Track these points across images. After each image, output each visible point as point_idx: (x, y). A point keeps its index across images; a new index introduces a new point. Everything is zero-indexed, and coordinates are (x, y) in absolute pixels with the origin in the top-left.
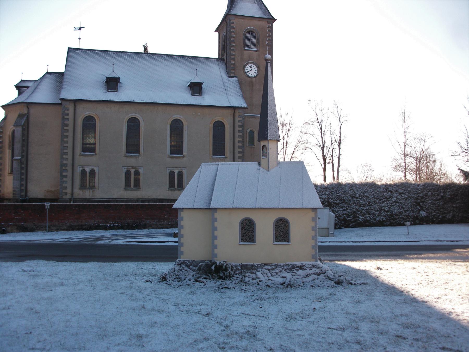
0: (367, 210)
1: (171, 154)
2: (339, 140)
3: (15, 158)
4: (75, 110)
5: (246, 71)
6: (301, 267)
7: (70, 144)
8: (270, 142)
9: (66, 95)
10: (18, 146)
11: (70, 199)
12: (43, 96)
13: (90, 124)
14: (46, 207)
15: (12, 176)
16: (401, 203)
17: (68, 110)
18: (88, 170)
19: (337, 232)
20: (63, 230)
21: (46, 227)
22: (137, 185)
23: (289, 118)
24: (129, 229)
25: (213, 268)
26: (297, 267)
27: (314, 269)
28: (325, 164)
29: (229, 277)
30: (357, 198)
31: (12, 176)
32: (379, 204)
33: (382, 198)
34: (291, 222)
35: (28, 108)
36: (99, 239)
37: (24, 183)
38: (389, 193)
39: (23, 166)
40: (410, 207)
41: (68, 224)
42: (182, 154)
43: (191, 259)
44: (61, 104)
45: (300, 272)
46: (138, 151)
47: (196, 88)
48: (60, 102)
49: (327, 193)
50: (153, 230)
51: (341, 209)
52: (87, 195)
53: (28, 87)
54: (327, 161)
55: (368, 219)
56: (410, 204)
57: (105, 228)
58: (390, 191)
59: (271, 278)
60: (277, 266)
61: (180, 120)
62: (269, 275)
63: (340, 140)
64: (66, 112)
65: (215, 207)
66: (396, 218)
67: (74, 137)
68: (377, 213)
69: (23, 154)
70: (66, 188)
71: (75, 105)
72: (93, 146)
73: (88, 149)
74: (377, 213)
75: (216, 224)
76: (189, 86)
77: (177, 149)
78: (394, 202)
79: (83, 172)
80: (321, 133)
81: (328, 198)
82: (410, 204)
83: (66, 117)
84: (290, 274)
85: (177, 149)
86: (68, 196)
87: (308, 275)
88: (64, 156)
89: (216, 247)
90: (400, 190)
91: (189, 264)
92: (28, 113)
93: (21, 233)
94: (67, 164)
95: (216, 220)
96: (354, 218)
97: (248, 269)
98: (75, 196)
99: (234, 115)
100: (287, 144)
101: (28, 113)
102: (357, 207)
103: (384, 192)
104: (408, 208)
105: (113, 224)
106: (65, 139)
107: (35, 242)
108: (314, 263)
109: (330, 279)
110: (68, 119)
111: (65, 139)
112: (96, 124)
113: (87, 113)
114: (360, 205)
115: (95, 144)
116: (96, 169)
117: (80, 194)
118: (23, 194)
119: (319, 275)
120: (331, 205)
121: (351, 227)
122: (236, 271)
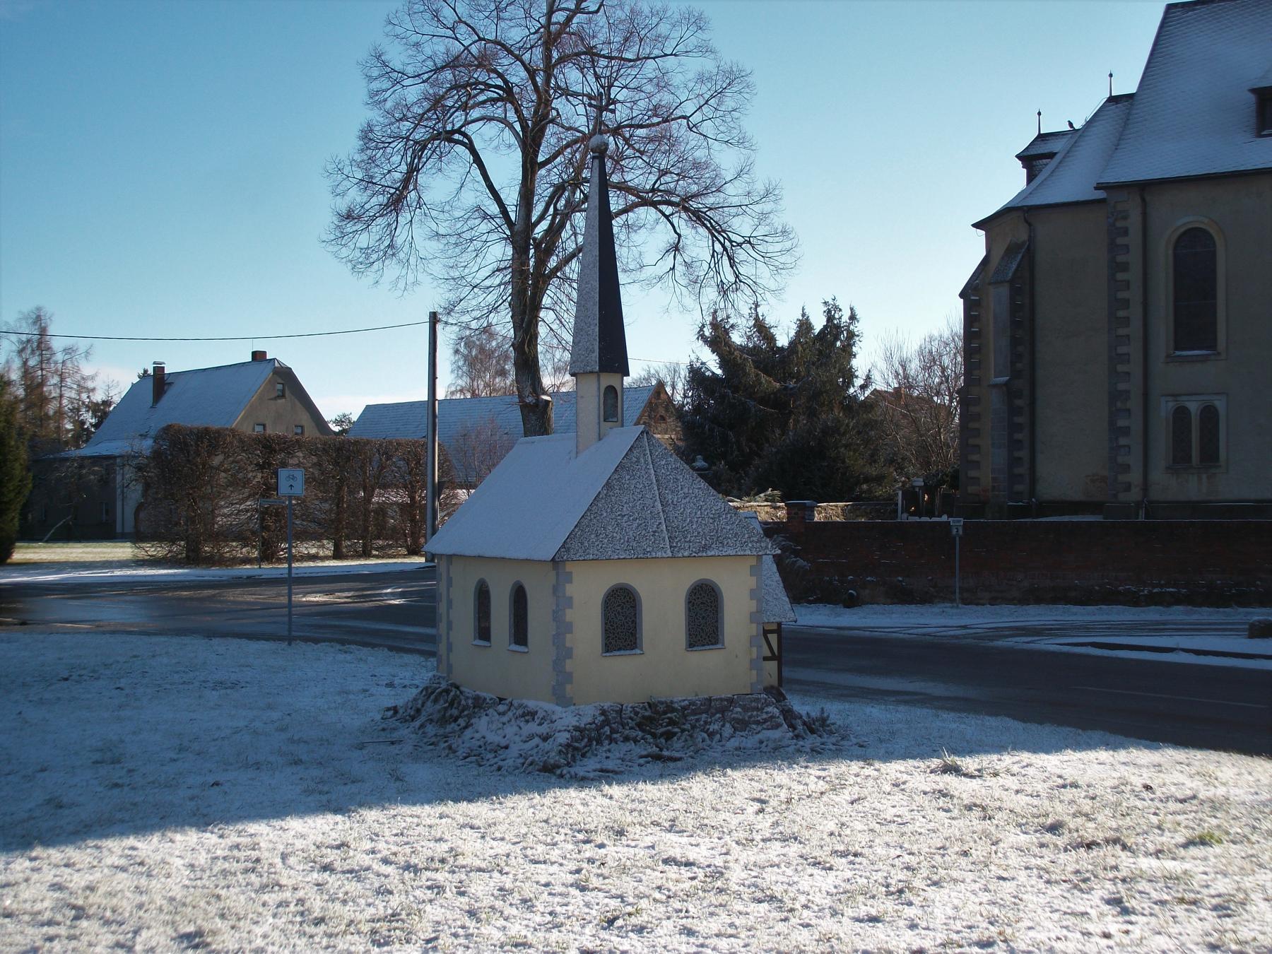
1: (1176, 349)
4: (1145, 215)
7: (1135, 329)
14: (954, 531)
17: (1125, 218)
18: (1194, 407)
22: (1210, 456)
24: (1210, 605)
35: (1030, 224)
36: (999, 633)
37: (1024, 454)
46: (1209, 341)
48: (1100, 194)
52: (1193, 488)
53: (1051, 155)
64: (1119, 224)
69: (1019, 365)
70: (1126, 468)
71: (1143, 200)
79: (1181, 414)
83: (1120, 241)
86: (1135, 495)
92: (1031, 239)
94: (1128, 392)
101: (1031, 239)
105: (1162, 586)
106: (1121, 314)
107: (842, 632)
110: (1127, 246)
111: (1121, 314)
113: (1185, 221)
116: (1220, 404)
117: (1172, 486)
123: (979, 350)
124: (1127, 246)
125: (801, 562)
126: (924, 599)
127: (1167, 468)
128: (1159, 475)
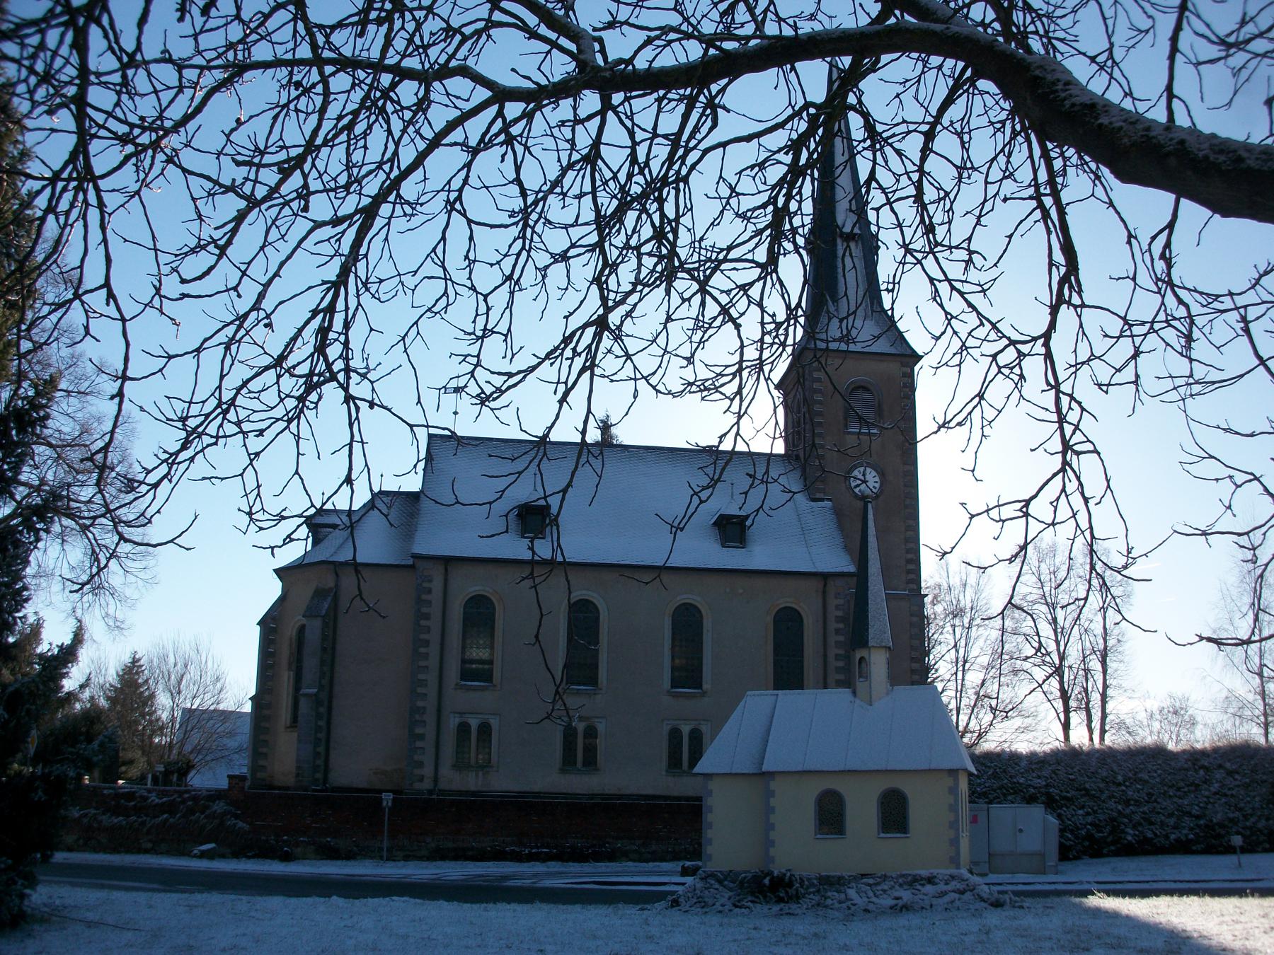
0: (1144, 813)
2: (1101, 646)
3: (304, 691)
5: (853, 484)
6: (931, 880)
7: (433, 662)
8: (873, 651)
9: (423, 546)
10: (311, 664)
11: (430, 792)
12: (374, 546)
13: (480, 614)
14: (385, 803)
15: (295, 735)
16: (1232, 795)
18: (474, 723)
19: (1067, 865)
20: (421, 858)
21: (381, 849)
22: (591, 761)
24: (574, 861)
25: (767, 881)
26: (922, 879)
27: (954, 883)
28: (1067, 711)
29: (797, 898)
30: (1119, 784)
31: (295, 735)
32: (1175, 800)
33: (1182, 784)
34: (909, 796)
35: (337, 575)
36: (506, 878)
37: (321, 749)
38: (1202, 772)
39: (322, 710)
40: (1257, 805)
41: (433, 845)
42: (699, 686)
43: (726, 869)
44: (412, 567)
45: (929, 888)
47: (732, 529)
48: (410, 562)
49: (1045, 773)
50: (630, 864)
51: (1081, 812)
52: (471, 782)
54: (1073, 704)
55: (1150, 835)
56: (1257, 799)
57: (517, 858)
58: (1203, 767)
59: (874, 899)
60: (885, 877)
61: (696, 607)
62: (870, 894)
63: (1106, 647)
64: (425, 585)
65: (771, 769)
66: (1223, 832)
67: (442, 644)
68: (1172, 821)
69: (323, 682)
71: (446, 570)
72: (486, 667)
73: (478, 674)
74: (1172, 821)
75: (773, 802)
76: (715, 524)
77: (688, 675)
78: (1216, 793)
79: (464, 729)
80: (1055, 631)
81: (1047, 786)
82: (1257, 799)
84: (909, 892)
85: (688, 675)
86: (427, 785)
87: (943, 894)
88: (419, 690)
89: (772, 843)
90: (1228, 765)
91: (722, 878)
92: (337, 586)
93: (325, 862)
94: (424, 708)
95: (772, 794)
96: (1111, 833)
97: (831, 884)
98: (443, 785)
99: (824, 592)
100: (965, 662)
102: (1120, 807)
103: (1187, 770)
104: (1253, 809)
108: (954, 871)
109: (983, 900)
111: (422, 650)
112: (494, 615)
114: (1127, 803)
115: (491, 662)
116: (494, 722)
117: (456, 781)
118: (319, 776)
119: (962, 892)
120: (1055, 801)
121: (1108, 855)
122: (808, 888)
123: (272, 666)
124: (430, 602)
125: (240, 824)
126: (350, 856)
127: (454, 766)
128: (446, 771)
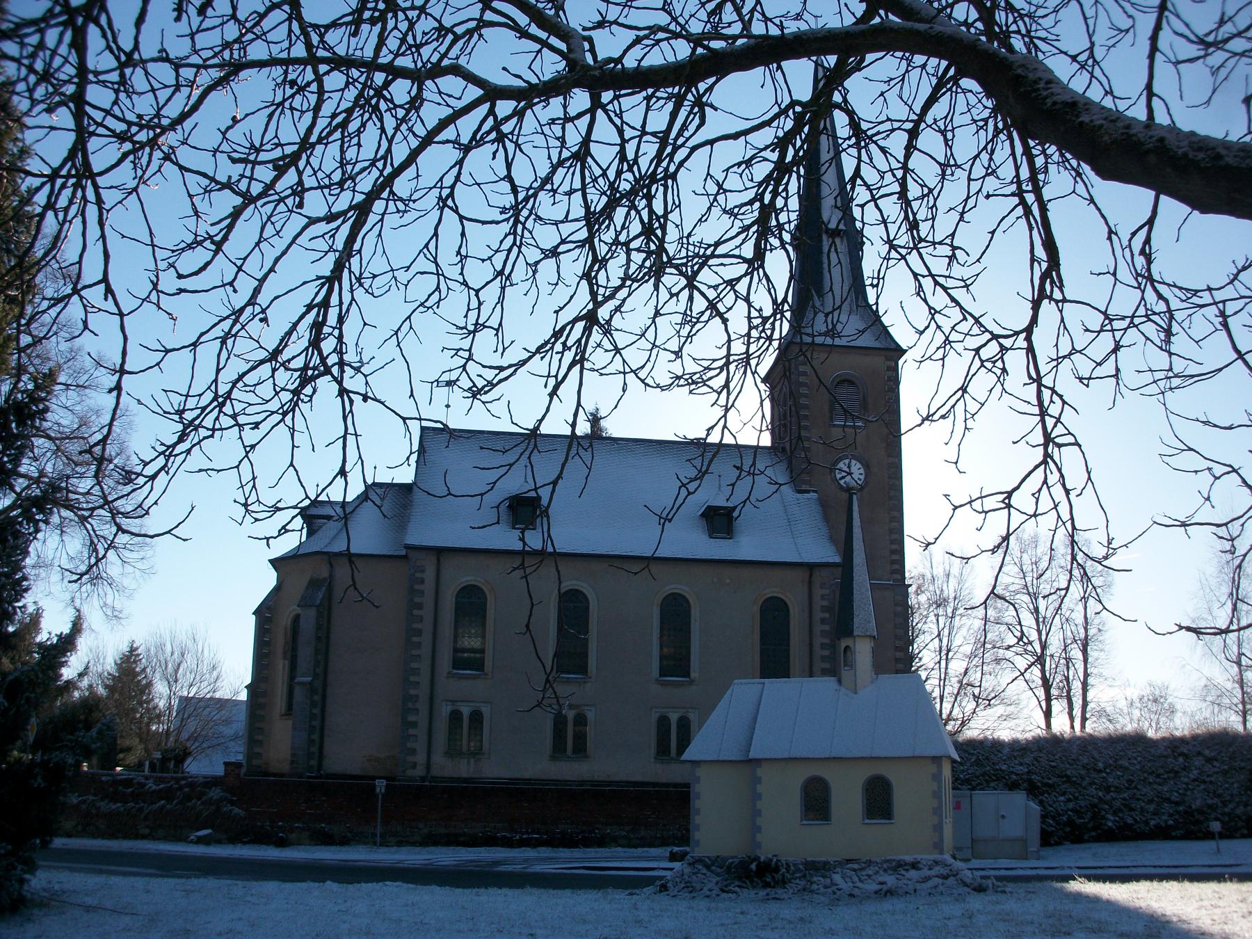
0: (1124, 799)
2: (1082, 636)
3: (299, 679)
6: (914, 865)
7: (426, 651)
8: (857, 640)
9: (416, 536)
10: (306, 653)
11: (423, 779)
12: (367, 537)
13: (472, 604)
14: (378, 790)
15: (290, 722)
16: (1211, 782)
18: (466, 711)
19: (1049, 851)
20: (413, 844)
21: (374, 835)
22: (580, 749)
23: (953, 583)
24: (564, 847)
25: (753, 866)
26: (906, 864)
27: (937, 868)
28: (1048, 699)
29: (783, 883)
30: (1100, 771)
31: (290, 722)
32: (1155, 786)
33: (1161, 771)
34: (893, 783)
35: (331, 565)
36: (497, 863)
37: (316, 737)
38: (1181, 759)
39: (316, 698)
40: (1235, 792)
41: (426, 831)
42: (687, 674)
43: (713, 854)
44: (405, 557)
45: (913, 874)
46: (583, 669)
48: (403, 553)
49: (1027, 760)
50: (619, 849)
51: (1062, 798)
52: (463, 769)
54: (1054, 692)
55: (1130, 821)
56: (1236, 785)
57: (508, 843)
58: (1182, 754)
59: (859, 884)
60: (869, 863)
62: (855, 879)
63: (1086, 636)
64: (418, 575)
65: (757, 756)
66: (1202, 818)
67: (435, 634)
68: (1152, 807)
69: (318, 670)
71: (439, 560)
72: (478, 655)
73: (470, 662)
74: (1152, 807)
75: (759, 788)
77: (676, 664)
78: (1195, 780)
79: (456, 716)
80: (1037, 620)
81: (1029, 772)
82: (1236, 785)
84: (893, 877)
85: (676, 664)
86: (419, 772)
87: (927, 879)
88: (412, 679)
89: (759, 829)
90: (1207, 752)
91: (710, 864)
92: (331, 576)
93: (319, 847)
94: (417, 696)
95: (759, 781)
96: (1092, 819)
97: (817, 870)
98: (435, 772)
99: (810, 582)
100: (949, 651)
102: (1100, 794)
103: (1166, 757)
108: (937, 857)
109: (966, 885)
111: (415, 639)
114: (1108, 789)
115: (482, 651)
116: (485, 710)
117: (448, 768)
118: (313, 763)
119: (945, 877)
121: (1089, 841)
122: (794, 873)
123: (267, 655)
124: (422, 592)
125: (236, 810)
126: (343, 842)
127: (446, 753)
128: (438, 758)
